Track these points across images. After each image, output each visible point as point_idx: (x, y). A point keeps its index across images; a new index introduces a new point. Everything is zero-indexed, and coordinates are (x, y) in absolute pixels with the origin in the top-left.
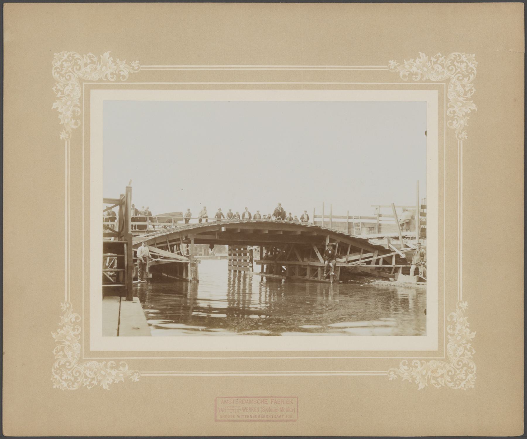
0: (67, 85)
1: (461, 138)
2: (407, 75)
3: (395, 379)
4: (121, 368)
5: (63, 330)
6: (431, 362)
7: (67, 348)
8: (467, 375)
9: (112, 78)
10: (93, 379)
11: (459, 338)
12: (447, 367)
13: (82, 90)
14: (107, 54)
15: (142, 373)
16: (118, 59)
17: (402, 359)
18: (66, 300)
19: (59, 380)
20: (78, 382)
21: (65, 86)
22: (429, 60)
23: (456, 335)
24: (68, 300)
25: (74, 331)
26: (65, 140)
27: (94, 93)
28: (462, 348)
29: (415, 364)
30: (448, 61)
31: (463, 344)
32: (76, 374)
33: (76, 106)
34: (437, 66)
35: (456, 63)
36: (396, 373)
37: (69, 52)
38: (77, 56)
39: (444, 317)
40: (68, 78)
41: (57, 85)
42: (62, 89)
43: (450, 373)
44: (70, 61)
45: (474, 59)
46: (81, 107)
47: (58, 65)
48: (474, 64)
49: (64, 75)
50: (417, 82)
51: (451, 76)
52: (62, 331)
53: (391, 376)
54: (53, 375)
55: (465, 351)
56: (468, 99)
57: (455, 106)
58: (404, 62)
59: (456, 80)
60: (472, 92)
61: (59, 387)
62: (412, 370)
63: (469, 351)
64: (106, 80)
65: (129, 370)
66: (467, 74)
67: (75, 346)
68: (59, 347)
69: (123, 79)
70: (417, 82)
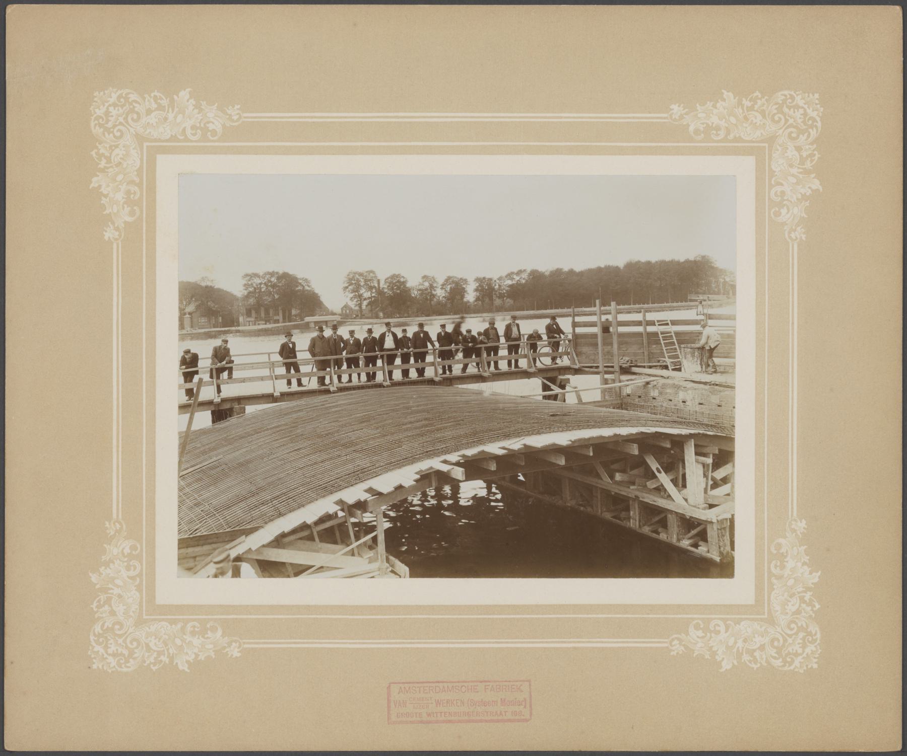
0: (117, 146)
1: (794, 238)
2: (702, 129)
3: (681, 652)
4: (210, 634)
5: (110, 569)
6: (743, 623)
7: (794, 162)
8: (804, 647)
9: (194, 135)
10: (751, 109)
11: (791, 582)
12: (141, 127)
13: (769, 604)
14: (726, 666)
15: (244, 643)
16: (706, 657)
17: (693, 619)
18: (115, 516)
19: (103, 655)
20: (134, 659)
21: (113, 148)
22: (740, 104)
23: (787, 577)
24: (118, 516)
25: (128, 571)
26: (797, 519)
27: (162, 160)
28: (114, 160)
29: (715, 627)
30: (138, 657)
31: (799, 593)
32: (132, 644)
33: (132, 182)
34: (159, 647)
35: (785, 110)
36: (683, 643)
37: (792, 669)
38: (133, 97)
39: (766, 547)
40: (118, 134)
41: (811, 612)
42: (107, 154)
43: (776, 644)
44: (122, 106)
45: (817, 102)
46: (140, 185)
47: (100, 112)
48: (817, 110)
49: (112, 130)
50: (718, 141)
51: (777, 132)
52: (108, 571)
53: (673, 648)
54: (92, 645)
55: (109, 155)
56: (807, 172)
57: (784, 183)
58: (215, 655)
59: (125, 623)
60: (813, 158)
61: (103, 666)
62: (200, 123)
63: (103, 154)
64: (182, 138)
65: (223, 638)
66: (805, 127)
67: (781, 166)
68: (103, 597)
69: (213, 137)
70: (718, 141)
